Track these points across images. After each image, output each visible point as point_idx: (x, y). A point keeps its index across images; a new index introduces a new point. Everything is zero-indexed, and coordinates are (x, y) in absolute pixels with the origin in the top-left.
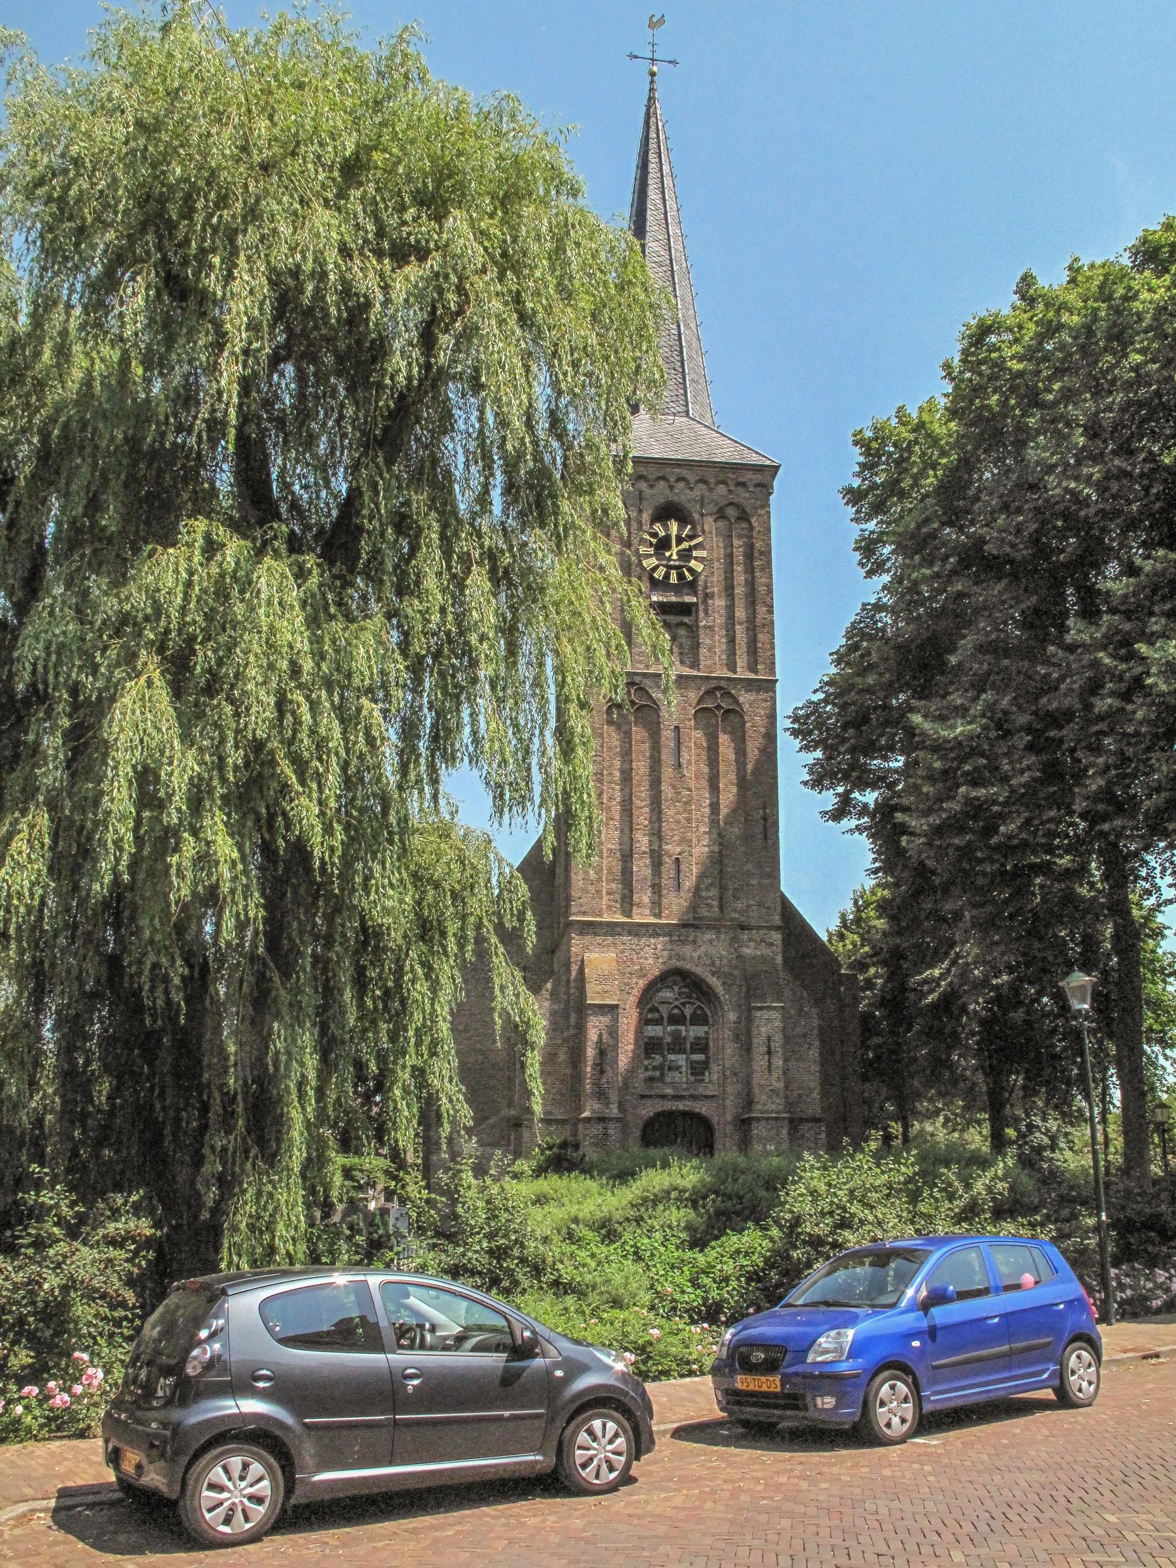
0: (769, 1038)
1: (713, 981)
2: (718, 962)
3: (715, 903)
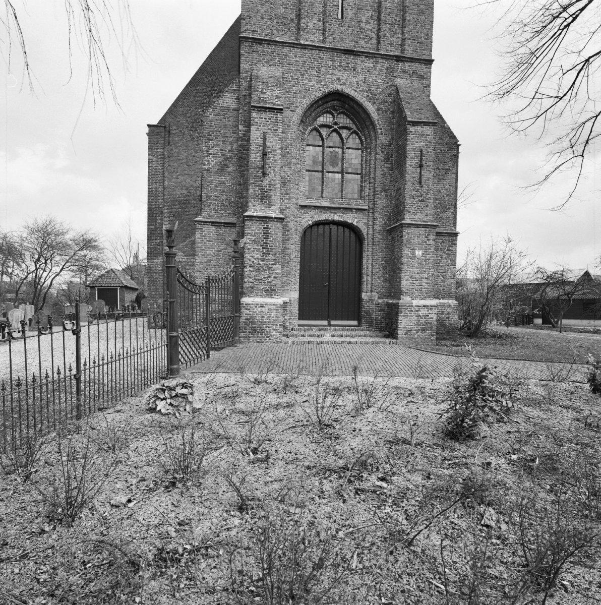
0: (421, 151)
1: (371, 108)
2: (374, 89)
3: (375, 36)
